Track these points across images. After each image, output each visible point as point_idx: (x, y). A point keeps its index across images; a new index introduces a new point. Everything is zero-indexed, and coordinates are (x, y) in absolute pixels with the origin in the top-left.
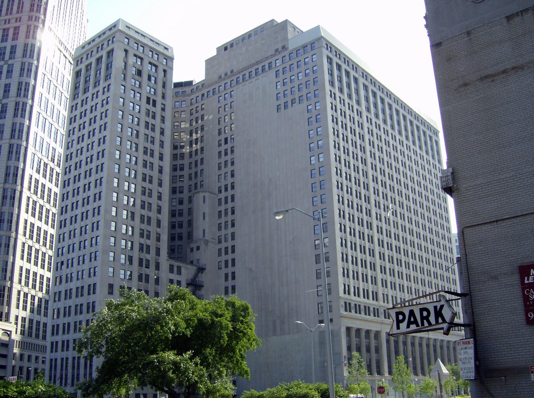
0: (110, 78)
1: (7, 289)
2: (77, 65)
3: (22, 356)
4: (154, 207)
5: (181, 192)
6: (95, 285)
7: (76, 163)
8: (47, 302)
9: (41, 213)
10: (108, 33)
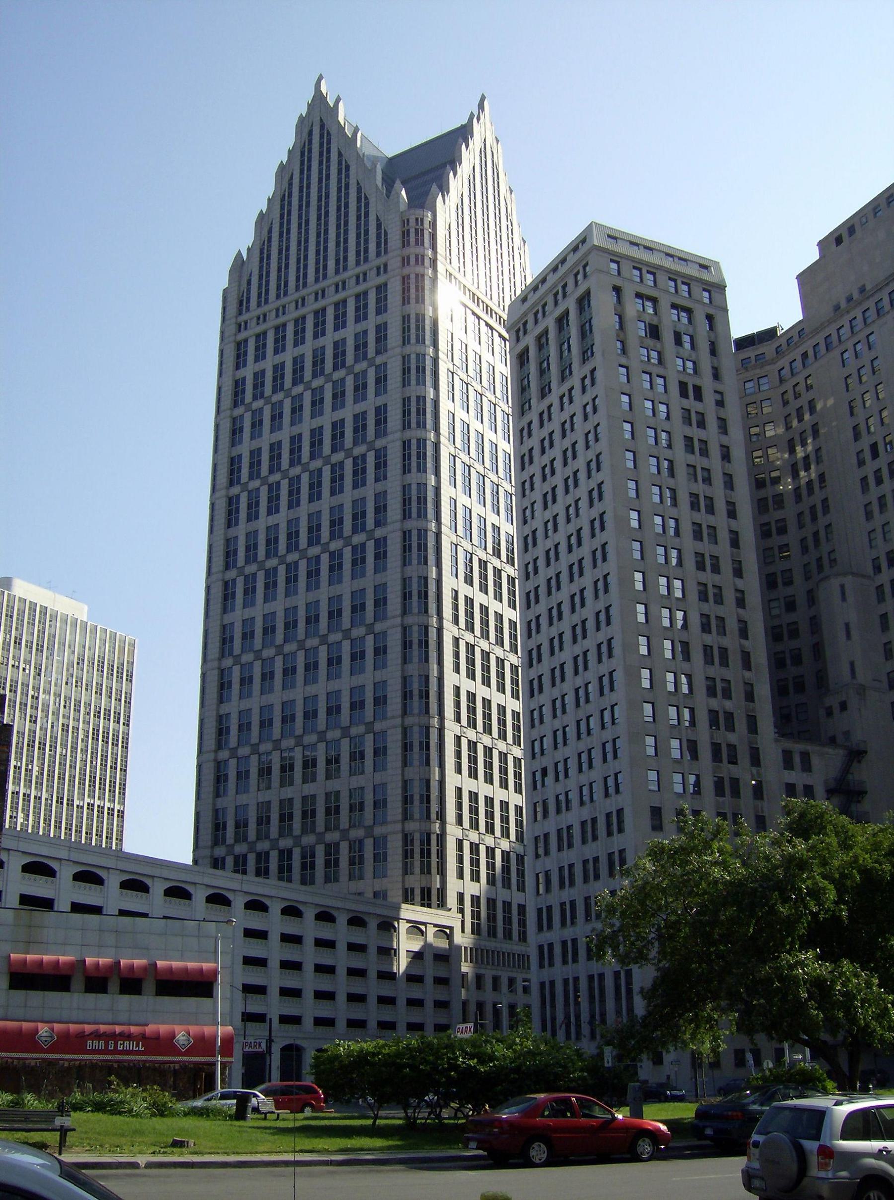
0: (592, 354)
1: (433, 838)
2: (518, 340)
3: (479, 978)
4: (732, 625)
5: (789, 583)
6: (620, 812)
7: (548, 552)
8: (520, 859)
9: (486, 669)
10: (572, 259)
